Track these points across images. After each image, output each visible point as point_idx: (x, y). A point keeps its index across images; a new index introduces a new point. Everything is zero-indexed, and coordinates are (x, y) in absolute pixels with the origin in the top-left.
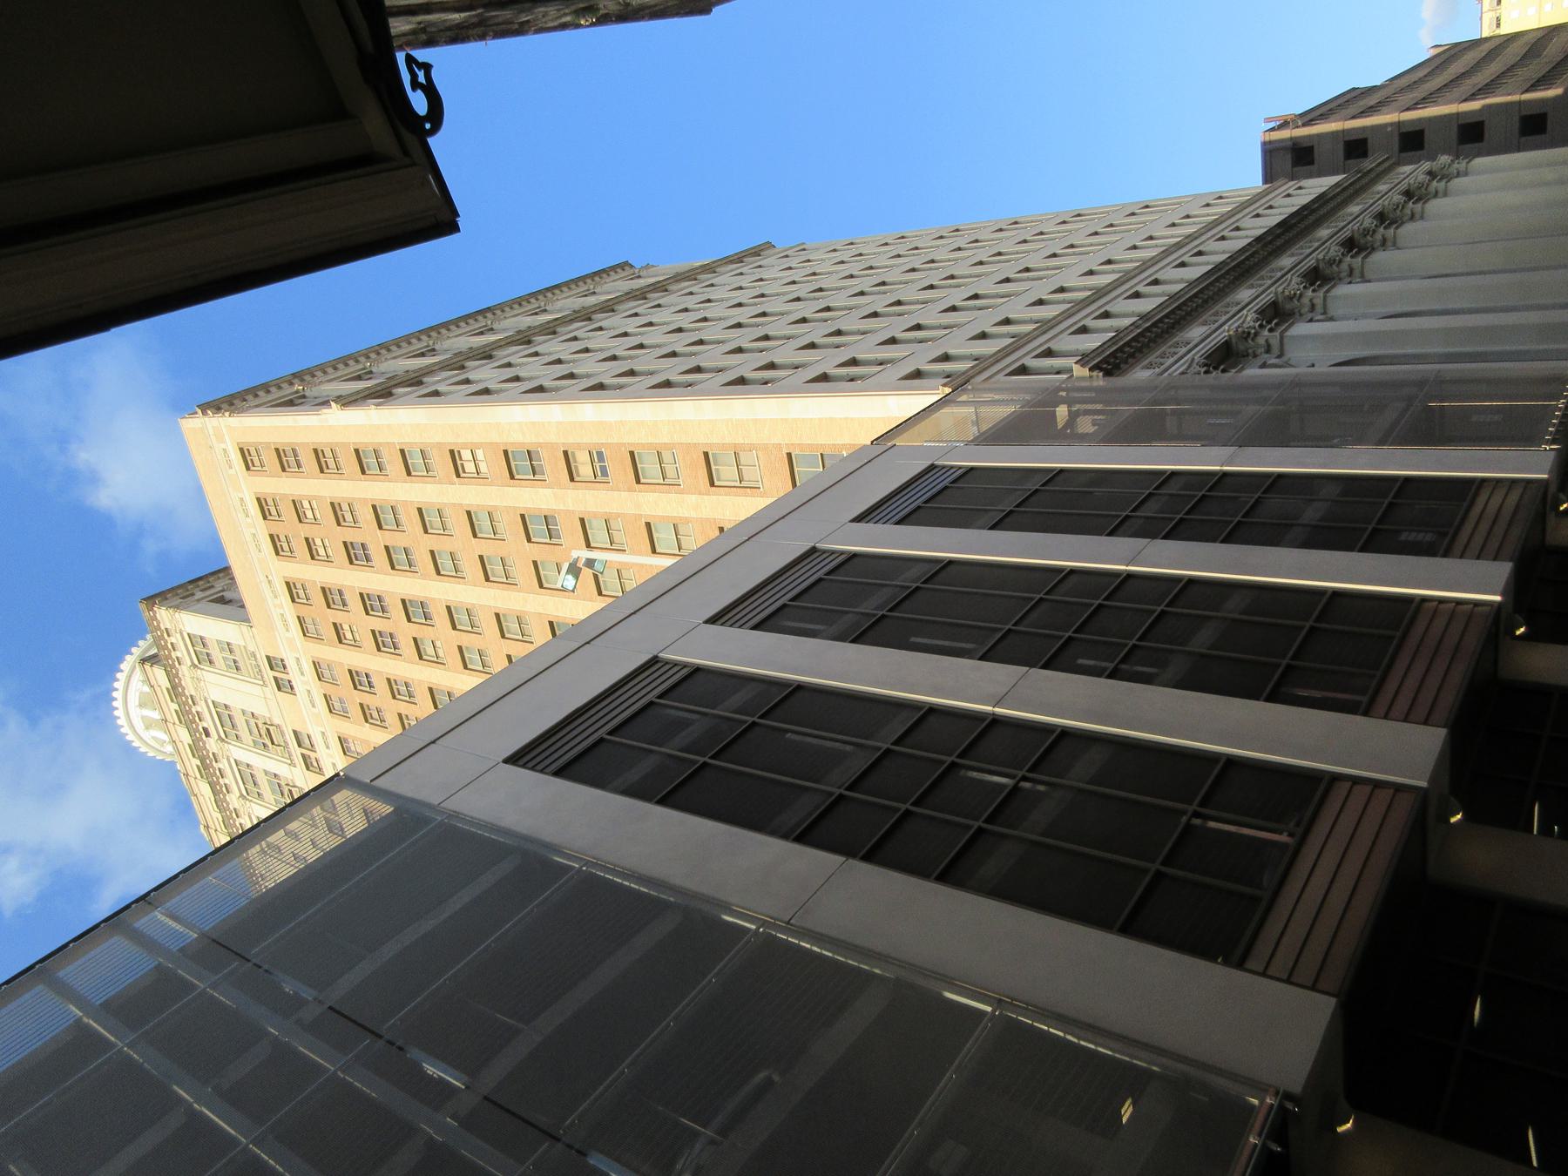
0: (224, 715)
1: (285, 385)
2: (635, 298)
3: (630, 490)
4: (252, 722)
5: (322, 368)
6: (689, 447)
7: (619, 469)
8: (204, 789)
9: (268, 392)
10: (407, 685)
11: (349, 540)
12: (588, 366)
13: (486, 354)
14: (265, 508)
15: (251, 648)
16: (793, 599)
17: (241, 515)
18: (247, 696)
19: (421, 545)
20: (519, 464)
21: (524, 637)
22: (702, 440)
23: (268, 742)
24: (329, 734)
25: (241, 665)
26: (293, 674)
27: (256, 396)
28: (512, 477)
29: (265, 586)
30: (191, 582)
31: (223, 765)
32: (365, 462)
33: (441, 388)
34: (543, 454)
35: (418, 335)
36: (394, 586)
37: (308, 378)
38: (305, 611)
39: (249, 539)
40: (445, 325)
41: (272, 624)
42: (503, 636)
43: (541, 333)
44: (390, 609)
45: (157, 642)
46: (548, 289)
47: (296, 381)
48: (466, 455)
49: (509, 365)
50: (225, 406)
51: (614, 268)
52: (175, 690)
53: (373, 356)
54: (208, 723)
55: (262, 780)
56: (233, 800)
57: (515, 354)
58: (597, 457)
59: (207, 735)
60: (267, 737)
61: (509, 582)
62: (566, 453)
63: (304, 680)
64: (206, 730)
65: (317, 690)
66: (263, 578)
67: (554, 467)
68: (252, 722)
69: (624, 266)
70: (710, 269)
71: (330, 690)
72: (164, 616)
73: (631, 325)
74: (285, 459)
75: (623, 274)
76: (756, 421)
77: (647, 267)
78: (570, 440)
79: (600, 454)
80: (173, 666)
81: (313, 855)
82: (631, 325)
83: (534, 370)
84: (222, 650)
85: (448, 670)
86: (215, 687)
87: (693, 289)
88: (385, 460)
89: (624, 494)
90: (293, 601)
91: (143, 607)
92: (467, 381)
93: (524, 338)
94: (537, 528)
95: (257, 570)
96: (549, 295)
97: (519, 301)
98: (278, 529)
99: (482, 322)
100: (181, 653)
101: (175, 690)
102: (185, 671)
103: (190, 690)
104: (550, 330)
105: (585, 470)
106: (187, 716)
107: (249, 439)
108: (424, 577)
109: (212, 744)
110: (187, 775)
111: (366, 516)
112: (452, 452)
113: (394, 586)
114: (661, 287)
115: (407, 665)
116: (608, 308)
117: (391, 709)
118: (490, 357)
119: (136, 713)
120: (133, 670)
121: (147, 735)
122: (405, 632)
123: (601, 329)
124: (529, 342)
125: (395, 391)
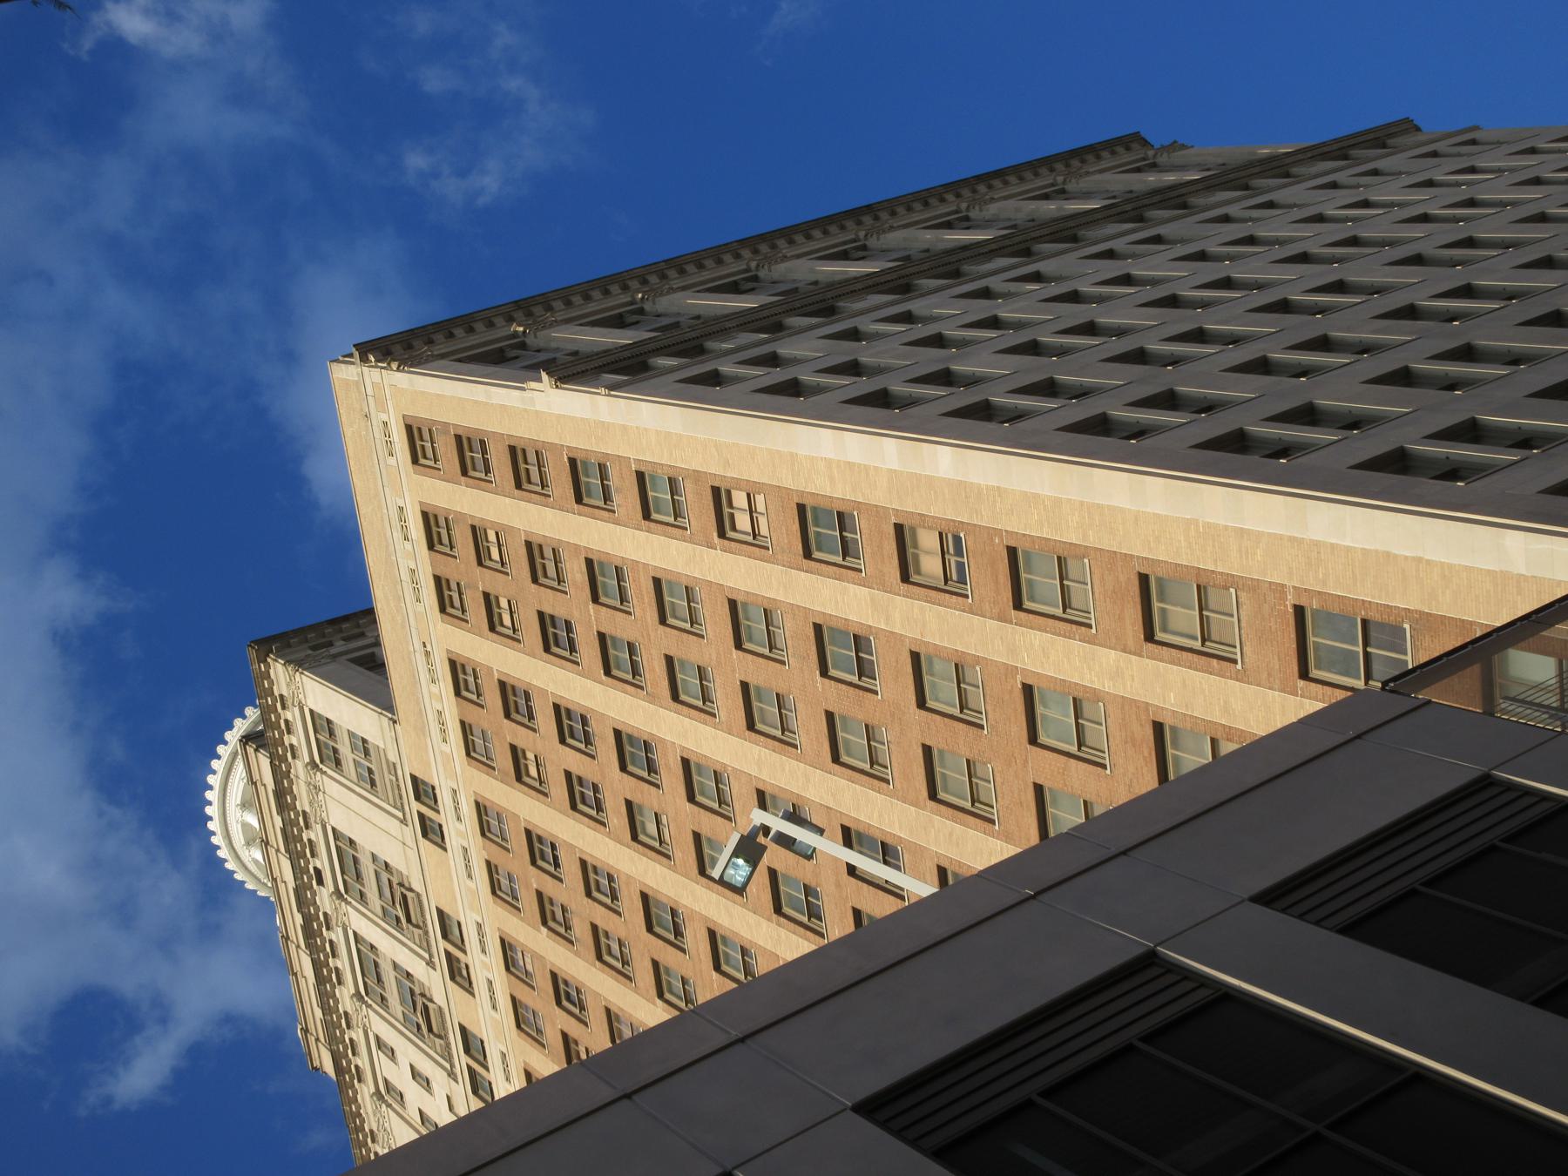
0: (346, 849)
1: (499, 321)
2: (1122, 217)
3: (1002, 618)
4: (384, 876)
5: (788, 233)
6: (1113, 558)
7: (987, 578)
8: (304, 963)
9: (471, 330)
10: (611, 878)
11: (548, 610)
12: (988, 363)
13: (950, 266)
14: (434, 528)
15: (393, 757)
16: (1511, 838)
17: (398, 535)
18: (382, 834)
19: (655, 643)
20: (824, 533)
21: (1084, 752)
22: (1138, 550)
23: (403, 920)
24: (487, 929)
25: (377, 777)
26: (446, 817)
27: (451, 335)
28: (807, 554)
29: (420, 659)
30: (332, 622)
31: (337, 935)
32: (586, 482)
33: (726, 368)
34: (862, 523)
35: (735, 248)
36: (610, 704)
37: (538, 310)
38: (473, 715)
39: (405, 576)
40: (986, 178)
41: (421, 728)
42: (1033, 739)
43: (1055, 237)
44: (597, 741)
45: (266, 712)
46: (979, 178)
47: (519, 315)
48: (740, 499)
49: (986, 294)
50: (397, 349)
51: (1111, 145)
52: (283, 796)
53: (653, 279)
54: (322, 862)
55: (389, 976)
56: (345, 996)
57: (1120, 235)
58: (952, 543)
59: (320, 882)
60: (402, 907)
61: (785, 740)
62: (899, 529)
63: (461, 830)
64: (318, 872)
65: (479, 852)
66: (418, 646)
67: (878, 551)
68: (384, 876)
69: (1133, 140)
70: (1279, 167)
71: (498, 857)
72: (280, 674)
73: (1214, 239)
74: (470, 455)
75: (1126, 157)
76: (1241, 532)
77: (1174, 146)
78: (911, 505)
79: (957, 539)
80: (284, 759)
81: (444, 1118)
82: (1214, 239)
83: (892, 354)
84: (354, 748)
85: (674, 869)
86: (341, 807)
87: (1339, 177)
88: (614, 482)
89: (992, 624)
90: (458, 693)
91: (252, 654)
92: (907, 318)
93: (1020, 244)
94: (841, 652)
95: (411, 627)
96: (1075, 163)
97: (924, 198)
98: (451, 570)
99: (852, 232)
100: (297, 739)
101: (283, 796)
102: (299, 768)
103: (303, 803)
104: (1067, 232)
105: (931, 565)
106: (297, 848)
107: (422, 412)
108: (652, 698)
109: (324, 898)
110: (287, 938)
111: (575, 573)
112: (716, 491)
113: (610, 704)
114: (1176, 199)
115: (611, 843)
116: (1067, 232)
117: (1012, 771)
118: (956, 274)
119: (236, 816)
120: (234, 755)
121: (245, 854)
122: (617, 787)
123: (1158, 240)
124: (1027, 253)
125: (710, 344)
